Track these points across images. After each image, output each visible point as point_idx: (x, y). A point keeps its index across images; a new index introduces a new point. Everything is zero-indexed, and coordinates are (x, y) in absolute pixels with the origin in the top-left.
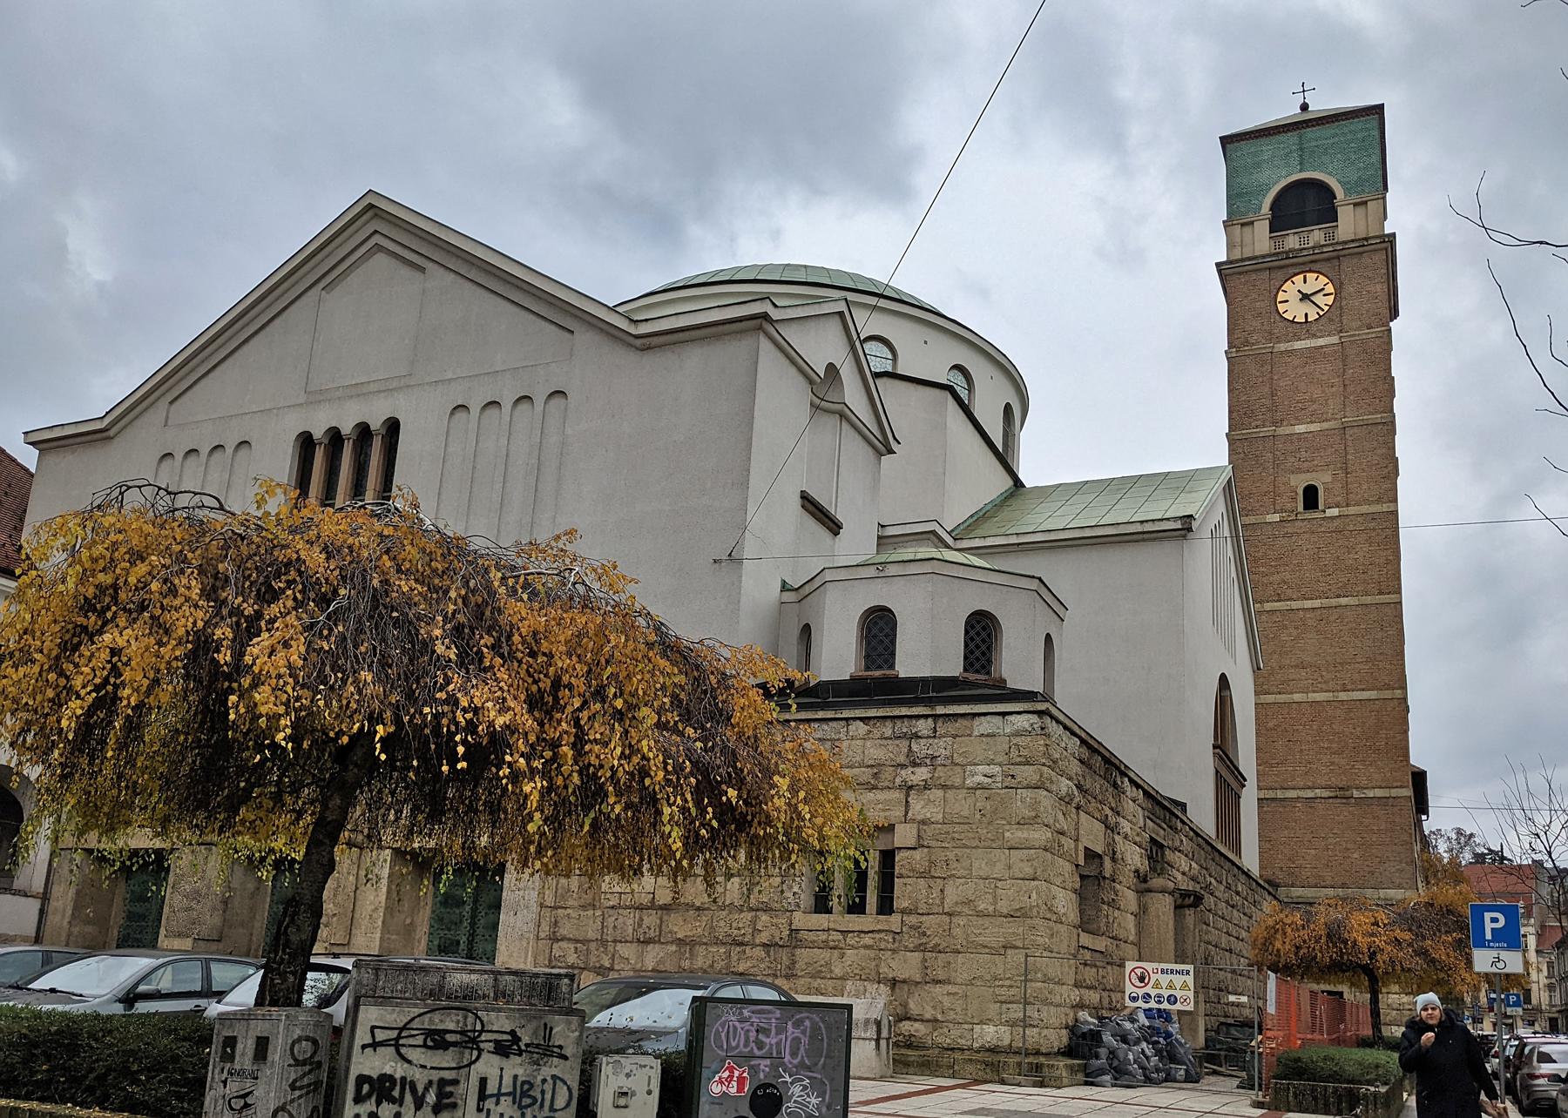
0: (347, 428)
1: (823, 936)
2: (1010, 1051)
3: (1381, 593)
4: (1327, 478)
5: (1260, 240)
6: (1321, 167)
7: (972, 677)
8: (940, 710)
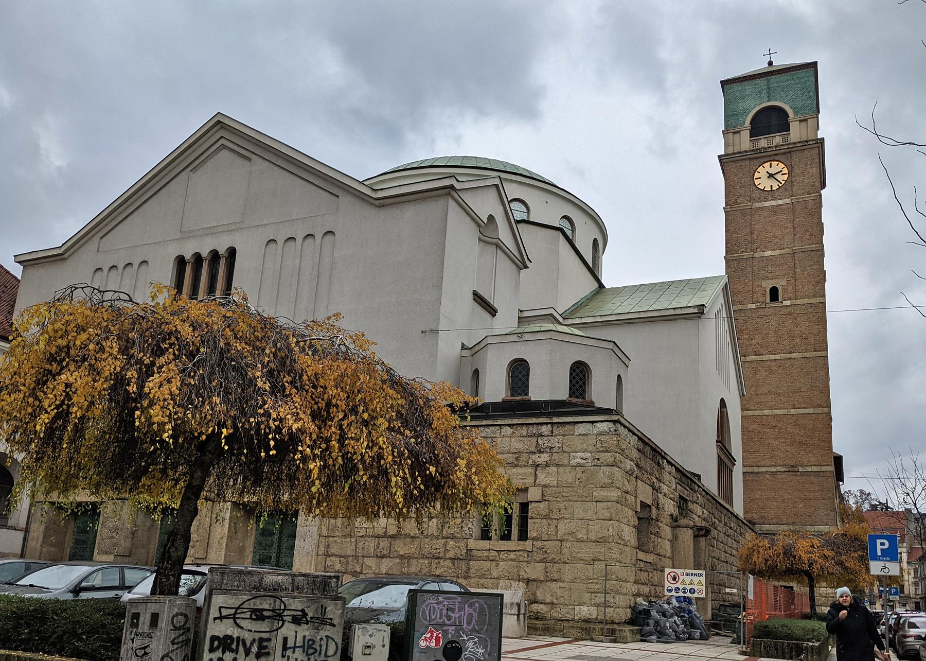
0: (205, 253)
1: (486, 554)
2: (597, 621)
3: (815, 351)
4: (784, 282)
5: (744, 142)
6: (780, 99)
7: (574, 400)
8: (555, 420)
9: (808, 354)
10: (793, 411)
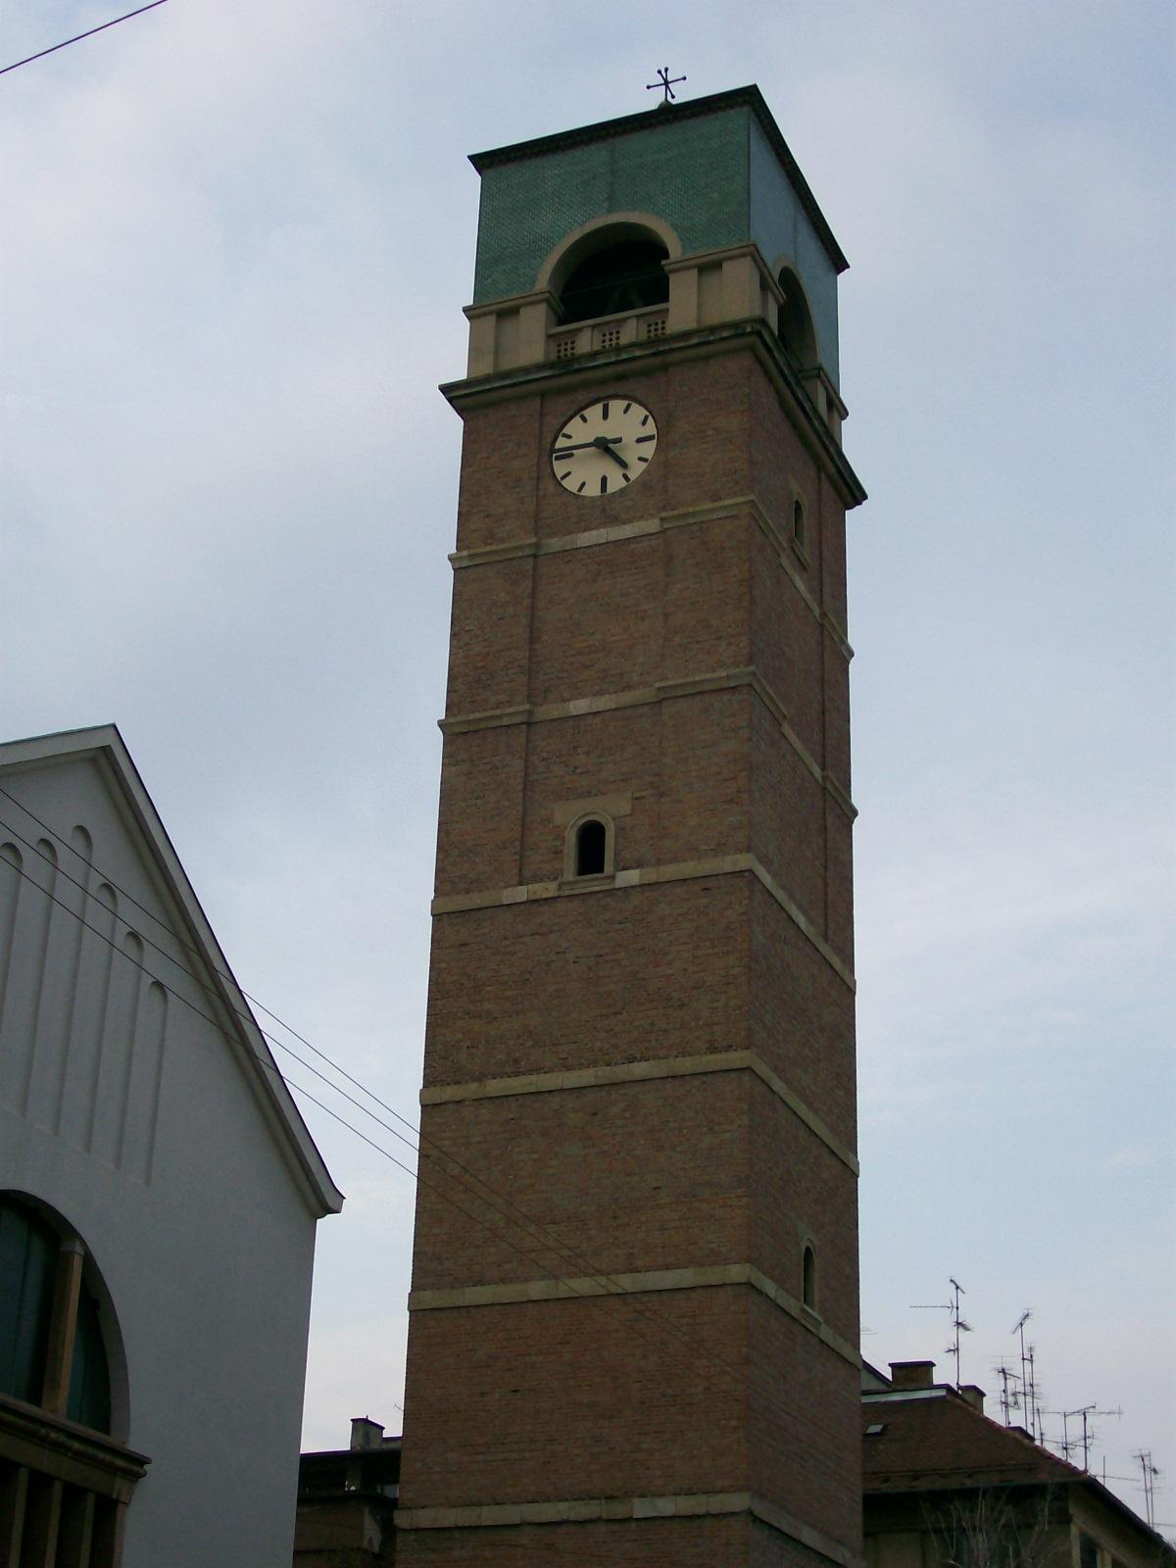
3: (713, 1049)
4: (624, 806)
5: (530, 340)
9: (686, 1064)
10: (627, 1282)
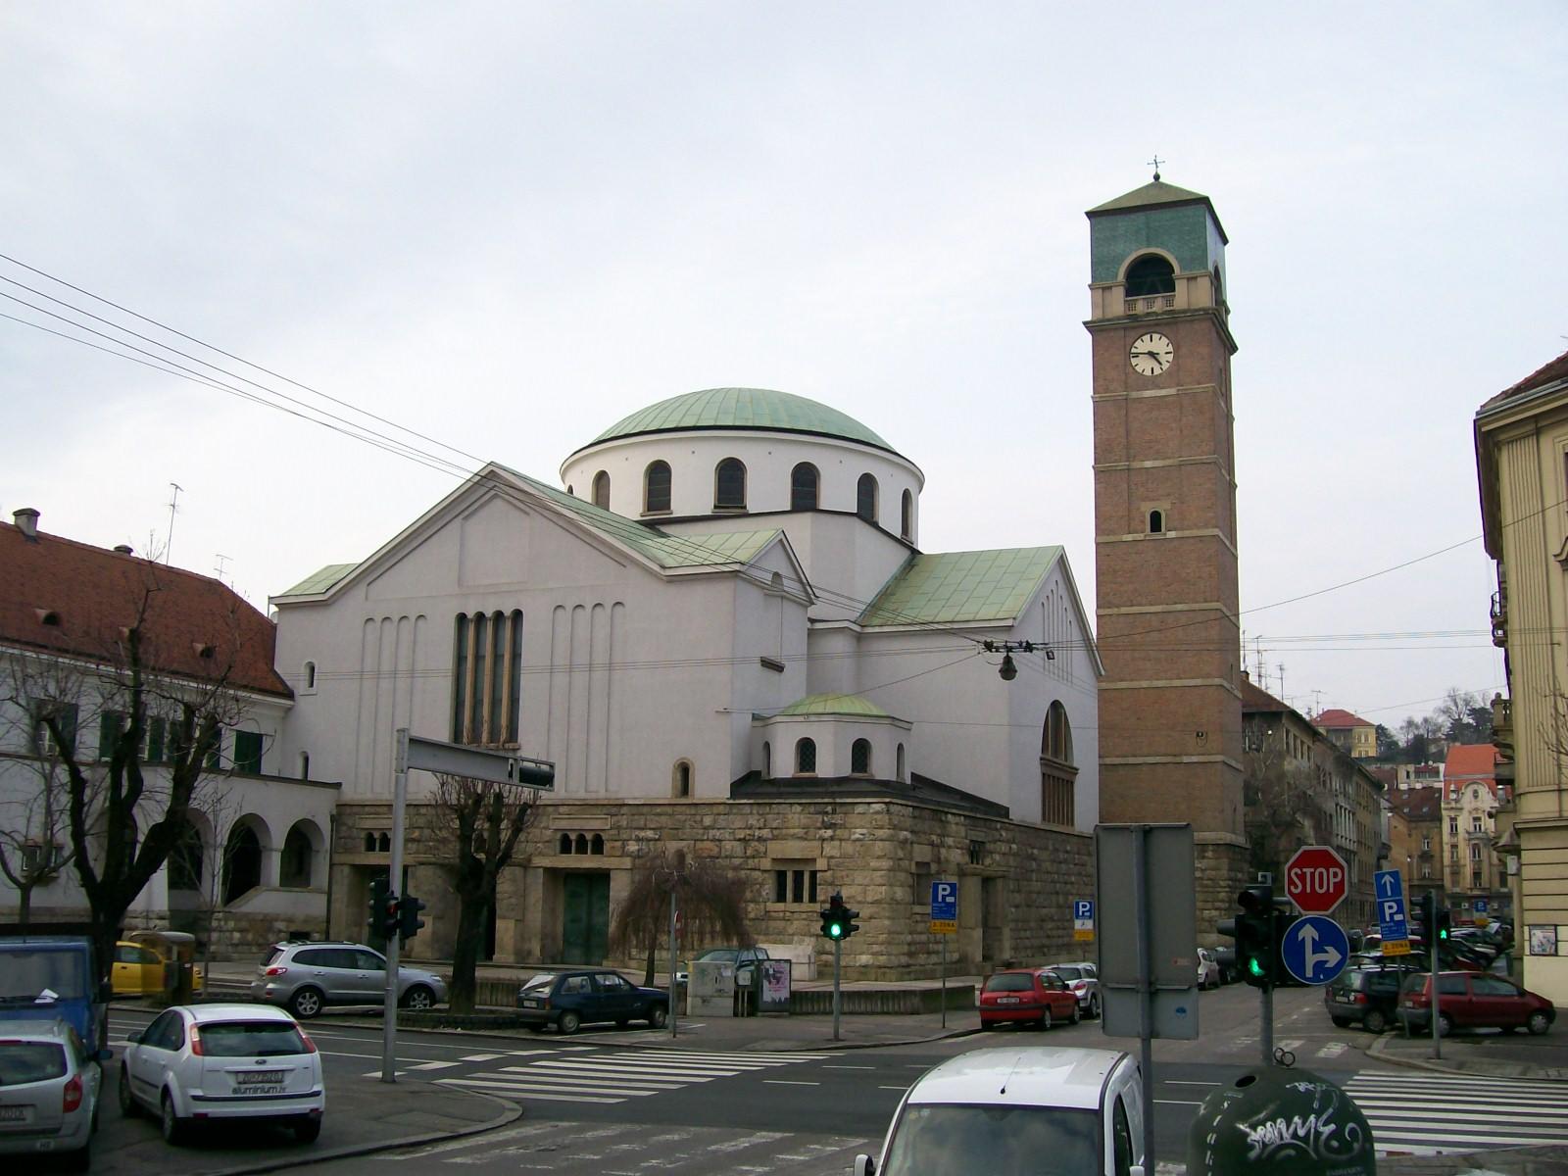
0: (489, 613)
1: (781, 914)
2: (872, 966)
3: (1206, 601)
4: (1167, 506)
5: (1117, 303)
6: (1162, 245)
7: (857, 775)
8: (838, 800)
